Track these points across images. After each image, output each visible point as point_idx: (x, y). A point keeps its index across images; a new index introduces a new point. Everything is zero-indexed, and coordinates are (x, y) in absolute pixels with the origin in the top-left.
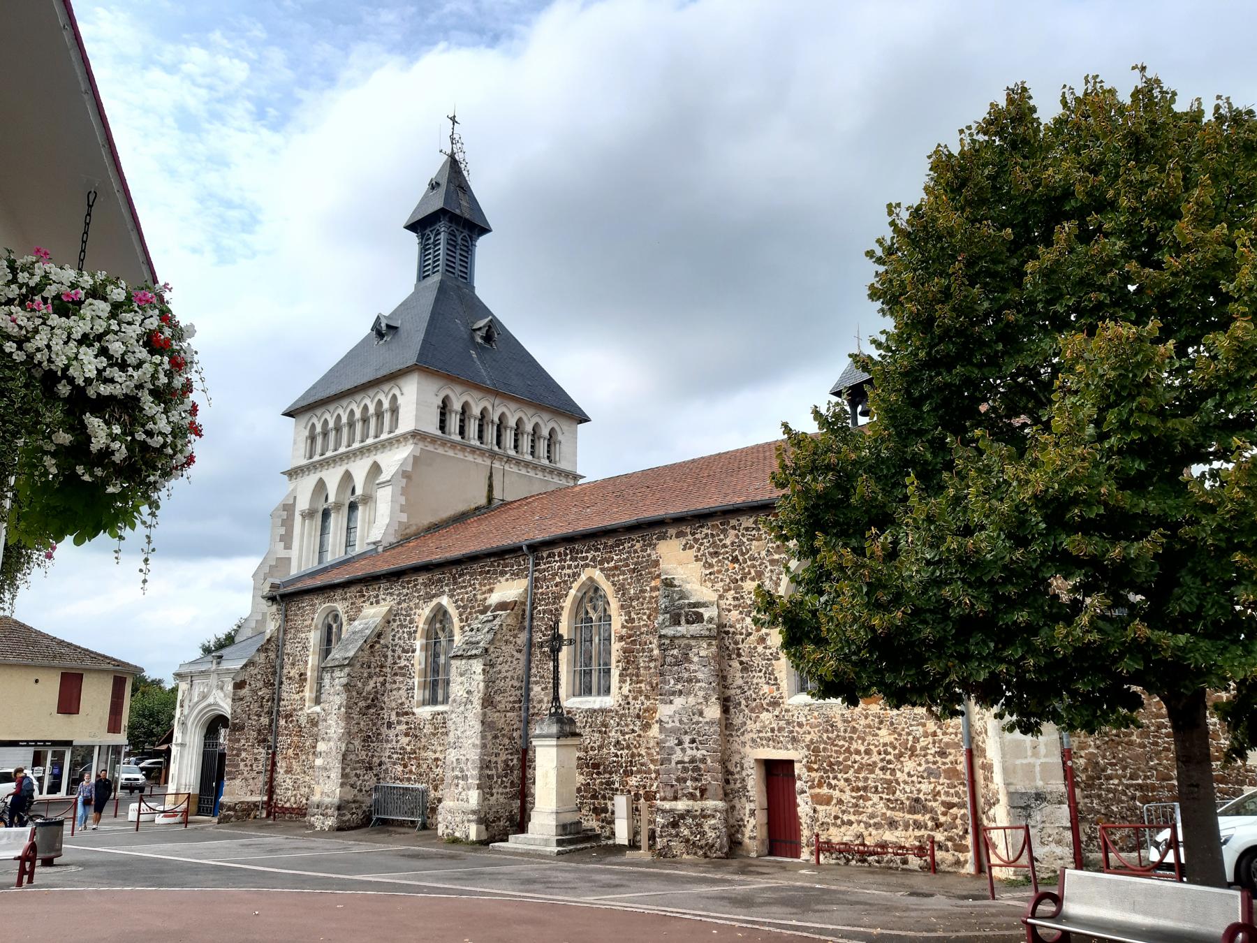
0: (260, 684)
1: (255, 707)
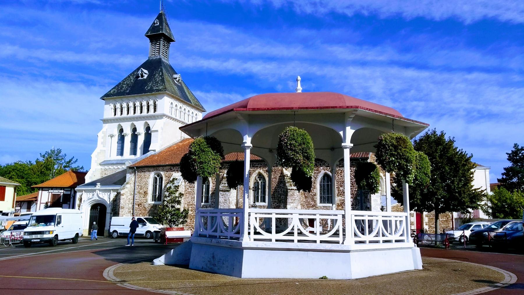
0: (129, 194)
1: (127, 202)
